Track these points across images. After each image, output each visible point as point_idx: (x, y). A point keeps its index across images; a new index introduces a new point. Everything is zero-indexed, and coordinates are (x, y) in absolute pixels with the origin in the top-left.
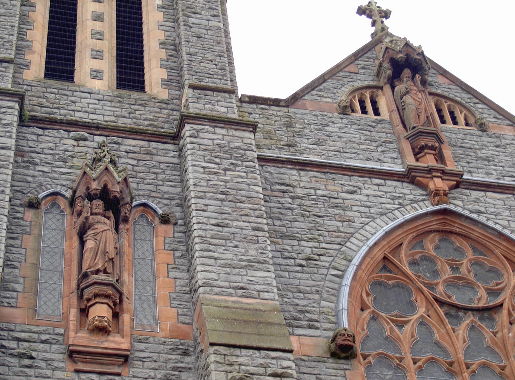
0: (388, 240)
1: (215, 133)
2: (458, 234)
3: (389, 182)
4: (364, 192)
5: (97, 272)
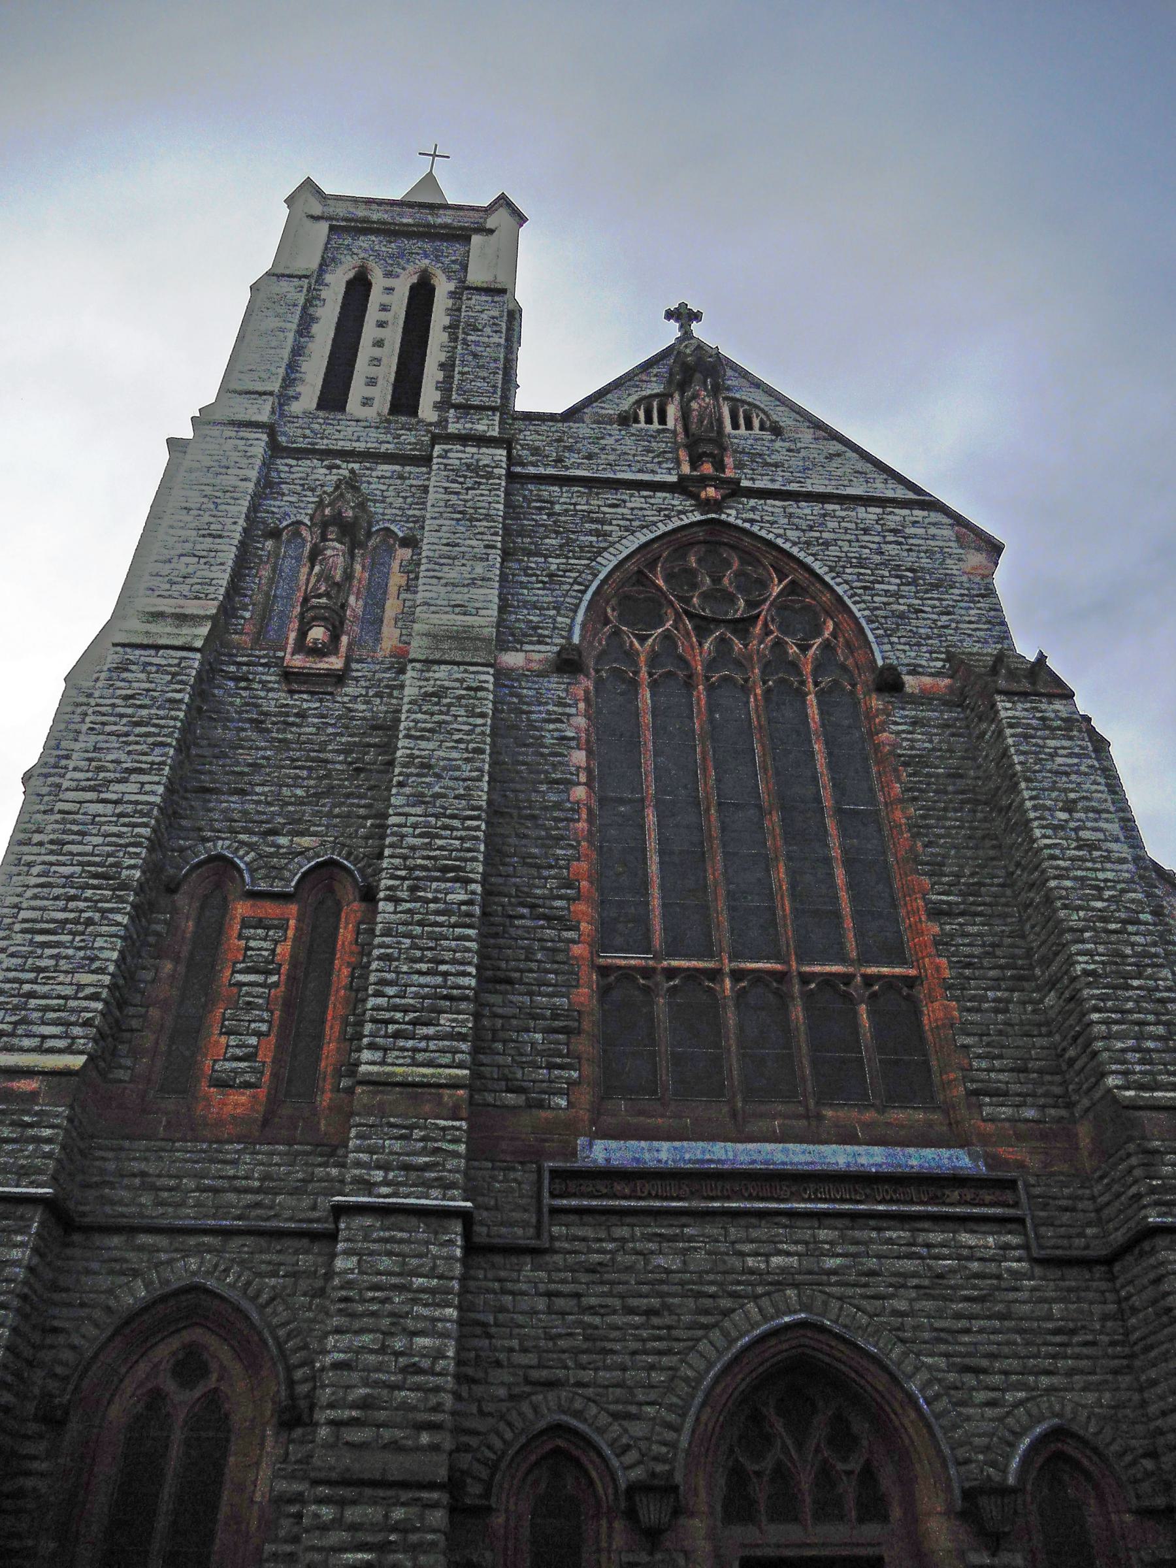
0: (644, 552)
1: (464, 452)
2: (725, 544)
3: (659, 494)
4: (629, 505)
5: (319, 596)
